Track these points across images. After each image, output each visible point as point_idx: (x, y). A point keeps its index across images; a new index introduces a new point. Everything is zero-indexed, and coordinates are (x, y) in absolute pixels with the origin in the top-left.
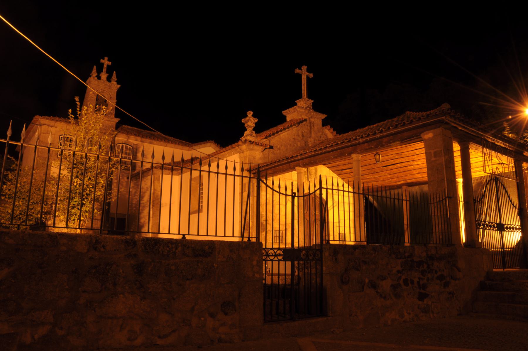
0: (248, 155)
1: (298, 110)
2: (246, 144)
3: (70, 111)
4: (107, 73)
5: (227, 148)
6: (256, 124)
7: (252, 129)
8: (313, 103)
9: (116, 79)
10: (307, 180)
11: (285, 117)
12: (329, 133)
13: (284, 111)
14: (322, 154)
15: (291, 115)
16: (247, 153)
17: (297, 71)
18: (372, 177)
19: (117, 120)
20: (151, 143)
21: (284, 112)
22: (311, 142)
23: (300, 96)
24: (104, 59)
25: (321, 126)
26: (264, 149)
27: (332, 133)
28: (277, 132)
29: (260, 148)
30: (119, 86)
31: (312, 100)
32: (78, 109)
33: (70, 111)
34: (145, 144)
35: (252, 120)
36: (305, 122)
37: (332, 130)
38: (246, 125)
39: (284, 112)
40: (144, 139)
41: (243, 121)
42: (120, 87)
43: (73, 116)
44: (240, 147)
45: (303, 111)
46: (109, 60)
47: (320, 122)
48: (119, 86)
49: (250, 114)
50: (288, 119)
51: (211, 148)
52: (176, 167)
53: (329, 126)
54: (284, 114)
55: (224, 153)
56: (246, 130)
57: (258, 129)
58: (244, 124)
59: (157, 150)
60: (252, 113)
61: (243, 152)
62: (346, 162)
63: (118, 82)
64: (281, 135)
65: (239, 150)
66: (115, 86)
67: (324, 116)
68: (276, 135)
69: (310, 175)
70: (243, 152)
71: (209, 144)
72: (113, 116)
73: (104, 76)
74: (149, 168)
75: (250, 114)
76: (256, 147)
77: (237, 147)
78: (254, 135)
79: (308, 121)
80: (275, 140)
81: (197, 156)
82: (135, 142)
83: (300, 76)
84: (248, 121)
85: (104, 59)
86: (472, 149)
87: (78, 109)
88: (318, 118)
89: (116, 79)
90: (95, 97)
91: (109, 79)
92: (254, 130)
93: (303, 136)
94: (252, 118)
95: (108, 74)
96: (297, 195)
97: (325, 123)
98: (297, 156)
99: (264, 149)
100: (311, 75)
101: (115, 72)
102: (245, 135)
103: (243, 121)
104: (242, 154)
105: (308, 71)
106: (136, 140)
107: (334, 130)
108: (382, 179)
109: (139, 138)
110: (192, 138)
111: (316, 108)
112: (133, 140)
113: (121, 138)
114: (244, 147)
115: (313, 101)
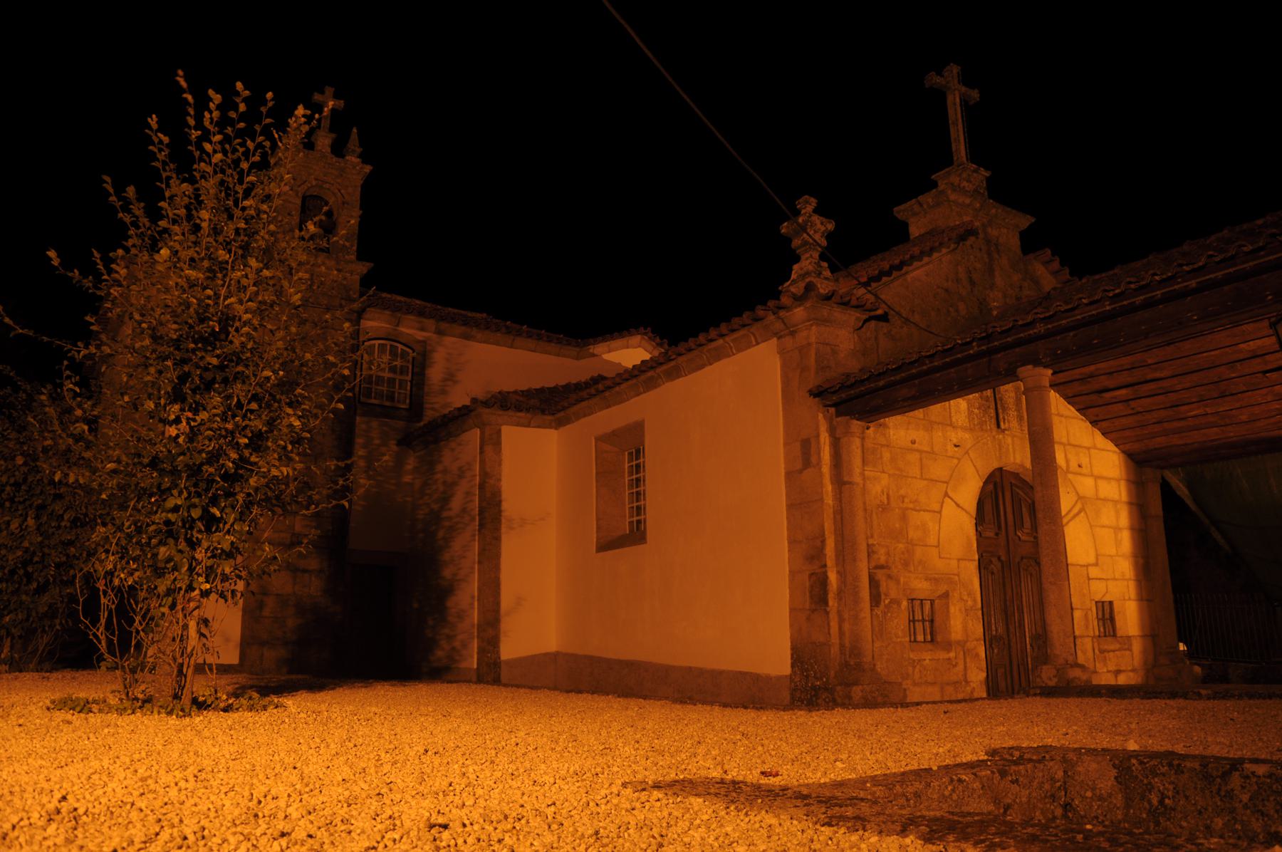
0: (813, 339)
1: (953, 197)
2: (808, 304)
3: (153, 121)
4: (331, 130)
5: (736, 321)
6: (829, 236)
7: (816, 255)
8: (988, 179)
9: (359, 150)
10: (994, 426)
11: (905, 225)
12: (1046, 273)
13: (902, 207)
14: (1148, 304)
15: (919, 217)
16: (812, 334)
17: (934, 80)
18: (1209, 410)
19: (363, 268)
20: (466, 337)
21: (900, 211)
22: (996, 302)
23: (945, 159)
24: (323, 93)
25: (1019, 251)
26: (866, 321)
27: (1054, 273)
28: (899, 267)
29: (853, 317)
30: (368, 169)
31: (987, 169)
32: (192, 122)
33: (153, 121)
34: (448, 340)
35: (819, 226)
36: (972, 239)
37: (1056, 265)
38: (796, 243)
39: (900, 211)
40: (444, 325)
41: (785, 228)
42: (371, 171)
43: (166, 140)
44: (782, 313)
45: (968, 201)
46: (336, 96)
47: (1015, 242)
48: (368, 169)
49: (808, 205)
50: (914, 231)
51: (640, 350)
52: (549, 404)
53: (1049, 252)
54: (901, 216)
55: (720, 341)
56: (797, 259)
57: (840, 255)
58: (789, 240)
59: (478, 362)
60: (814, 202)
61: (792, 334)
62: (1125, 361)
63: (365, 158)
64: (909, 277)
65: (778, 326)
66: (355, 169)
67: (1025, 221)
68: (895, 274)
69: (1004, 409)
70: (792, 334)
71: (636, 339)
72: (353, 257)
73: (324, 141)
74: (465, 407)
75: (808, 205)
76: (838, 314)
77: (772, 317)
78: (827, 273)
79: (981, 236)
80: (892, 292)
81: (605, 374)
82: (420, 335)
83: (940, 96)
84: (803, 229)
85: (323, 93)
86: (970, 405)
87: (192, 122)
88: (1008, 226)
89: (359, 150)
90: (299, 202)
91: (338, 149)
92: (823, 257)
93: (972, 283)
94: (816, 219)
95: (334, 135)
96: (46, 542)
97: (1030, 242)
98: (1031, 324)
99: (866, 321)
100: (975, 95)
101: (355, 130)
102: (794, 276)
103: (785, 228)
104: (788, 342)
105: (966, 80)
106: (422, 329)
107: (1062, 264)
108: (1244, 418)
109: (430, 323)
110: (582, 324)
111: (999, 191)
112: (410, 329)
113: (375, 323)
114: (799, 313)
115: (987, 174)
